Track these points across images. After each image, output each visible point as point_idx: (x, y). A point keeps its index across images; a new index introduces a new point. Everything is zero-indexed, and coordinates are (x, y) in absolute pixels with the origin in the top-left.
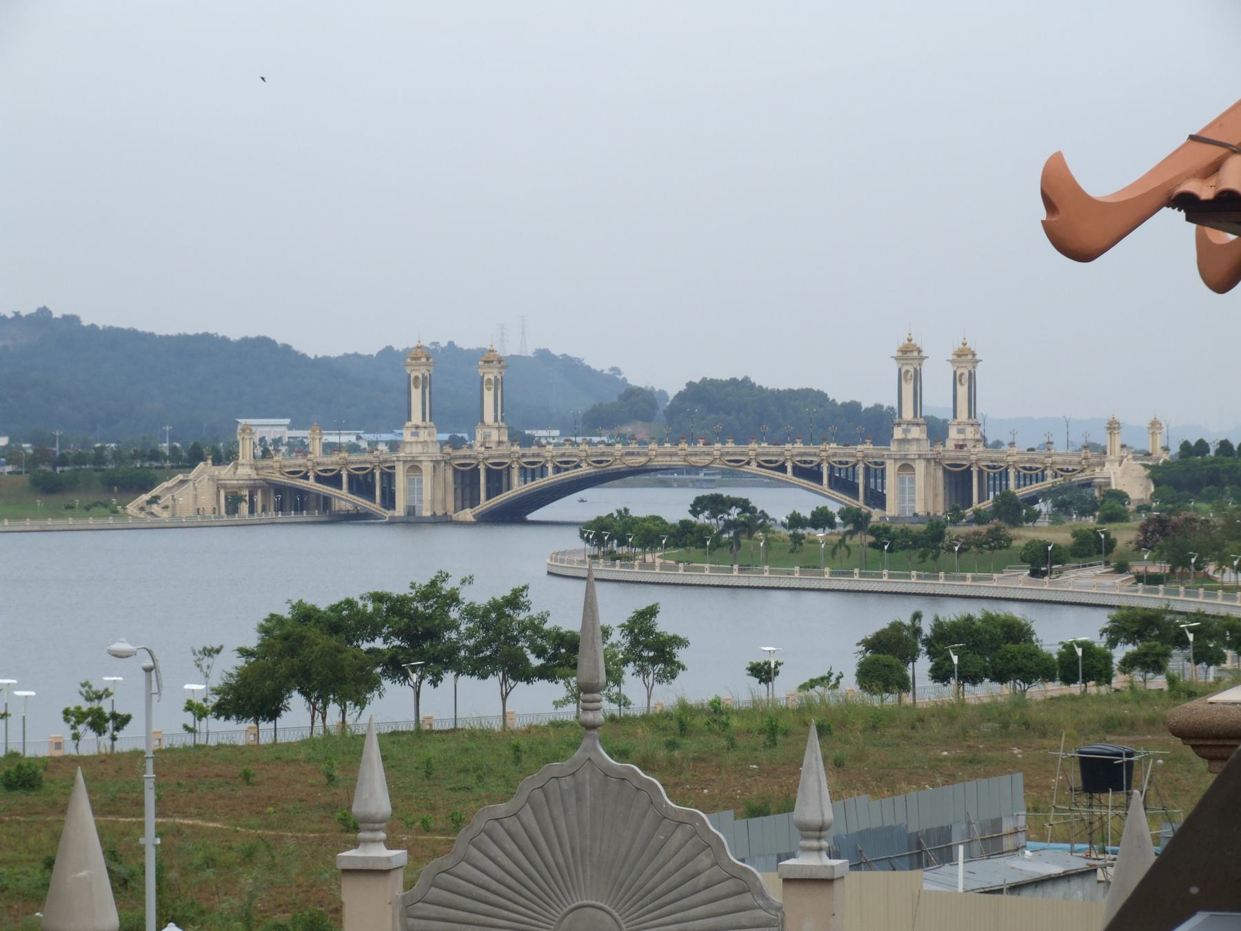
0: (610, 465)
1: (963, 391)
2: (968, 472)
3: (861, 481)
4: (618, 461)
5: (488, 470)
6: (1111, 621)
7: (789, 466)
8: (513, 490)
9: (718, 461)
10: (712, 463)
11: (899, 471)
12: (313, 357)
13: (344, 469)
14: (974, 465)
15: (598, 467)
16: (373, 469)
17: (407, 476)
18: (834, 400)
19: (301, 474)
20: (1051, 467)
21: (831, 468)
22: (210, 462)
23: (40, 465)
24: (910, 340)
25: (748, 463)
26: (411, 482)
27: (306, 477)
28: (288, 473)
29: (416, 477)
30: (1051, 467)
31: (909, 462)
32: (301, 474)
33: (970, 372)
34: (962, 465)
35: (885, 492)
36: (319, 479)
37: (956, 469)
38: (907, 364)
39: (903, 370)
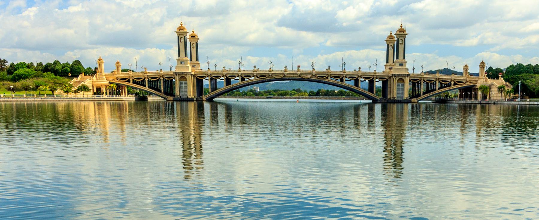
0: (267, 78)
2: (479, 76)
4: (270, 76)
5: (164, 81)
7: (131, 80)
8: (231, 85)
9: (314, 77)
10: (311, 77)
11: (397, 81)
13: (146, 78)
14: (146, 78)
15: (261, 79)
17: (180, 81)
19: (127, 80)
20: (241, 75)
22: (83, 74)
24: (181, 25)
25: (327, 78)
26: (181, 83)
27: (129, 81)
29: (183, 82)
30: (241, 75)
31: (184, 75)
32: (127, 80)
33: (196, 43)
34: (156, 78)
36: (134, 82)
37: (155, 79)
38: (401, 37)
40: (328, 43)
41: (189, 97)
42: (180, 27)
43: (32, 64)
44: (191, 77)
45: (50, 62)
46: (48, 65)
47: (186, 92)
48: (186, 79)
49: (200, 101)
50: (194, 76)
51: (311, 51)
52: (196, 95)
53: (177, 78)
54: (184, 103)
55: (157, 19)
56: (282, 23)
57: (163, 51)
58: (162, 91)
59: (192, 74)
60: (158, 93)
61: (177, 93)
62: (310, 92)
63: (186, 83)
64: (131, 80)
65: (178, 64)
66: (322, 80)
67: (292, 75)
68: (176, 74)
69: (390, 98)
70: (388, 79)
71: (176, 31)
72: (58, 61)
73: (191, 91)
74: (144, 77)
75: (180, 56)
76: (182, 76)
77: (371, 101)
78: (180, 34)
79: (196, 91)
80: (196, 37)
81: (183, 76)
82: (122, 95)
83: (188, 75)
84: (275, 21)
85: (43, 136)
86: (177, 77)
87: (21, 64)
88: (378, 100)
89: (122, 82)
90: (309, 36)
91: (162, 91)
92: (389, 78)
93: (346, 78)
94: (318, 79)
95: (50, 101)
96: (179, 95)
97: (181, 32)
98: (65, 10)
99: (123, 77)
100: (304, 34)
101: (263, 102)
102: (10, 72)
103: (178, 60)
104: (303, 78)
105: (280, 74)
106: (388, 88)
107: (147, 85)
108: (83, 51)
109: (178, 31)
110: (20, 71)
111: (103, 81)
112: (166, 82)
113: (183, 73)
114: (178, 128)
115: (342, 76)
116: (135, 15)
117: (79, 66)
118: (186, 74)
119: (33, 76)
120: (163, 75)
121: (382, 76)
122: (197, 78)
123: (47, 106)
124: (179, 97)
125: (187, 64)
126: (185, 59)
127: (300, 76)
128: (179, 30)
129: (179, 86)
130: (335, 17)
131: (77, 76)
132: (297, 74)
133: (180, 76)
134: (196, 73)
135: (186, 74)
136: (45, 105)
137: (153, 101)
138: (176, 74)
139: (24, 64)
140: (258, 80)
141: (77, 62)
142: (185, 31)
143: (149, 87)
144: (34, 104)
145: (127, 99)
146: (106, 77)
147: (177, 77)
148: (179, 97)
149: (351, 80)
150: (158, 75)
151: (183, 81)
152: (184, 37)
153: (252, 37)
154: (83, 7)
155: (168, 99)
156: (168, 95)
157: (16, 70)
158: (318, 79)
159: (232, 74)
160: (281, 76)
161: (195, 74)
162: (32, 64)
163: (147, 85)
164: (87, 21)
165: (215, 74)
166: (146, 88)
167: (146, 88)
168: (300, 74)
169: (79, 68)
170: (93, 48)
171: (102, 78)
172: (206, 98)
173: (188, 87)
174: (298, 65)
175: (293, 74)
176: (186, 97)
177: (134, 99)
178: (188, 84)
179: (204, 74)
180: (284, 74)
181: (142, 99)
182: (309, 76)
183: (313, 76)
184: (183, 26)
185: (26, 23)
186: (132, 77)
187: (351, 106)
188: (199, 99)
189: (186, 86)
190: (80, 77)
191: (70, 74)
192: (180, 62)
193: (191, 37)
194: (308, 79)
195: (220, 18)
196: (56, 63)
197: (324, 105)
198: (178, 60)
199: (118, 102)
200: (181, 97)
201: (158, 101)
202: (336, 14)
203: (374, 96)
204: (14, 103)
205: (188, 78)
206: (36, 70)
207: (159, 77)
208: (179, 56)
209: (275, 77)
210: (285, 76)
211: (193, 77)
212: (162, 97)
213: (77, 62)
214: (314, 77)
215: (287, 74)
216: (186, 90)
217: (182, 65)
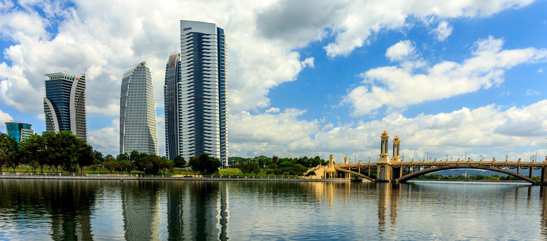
0: (444, 166)
1: (396, 149)
3: (369, 173)
6: (217, 200)
7: (350, 168)
9: (481, 166)
12: (463, 108)
15: (439, 167)
16: (368, 167)
18: (109, 156)
21: (361, 169)
22: (321, 165)
23: (525, 153)
24: (385, 132)
26: (381, 170)
27: (348, 169)
28: (536, 166)
33: (398, 144)
35: (376, 176)
36: (351, 170)
39: (383, 140)
40: (533, 144)
41: (386, 179)
42: (384, 134)
43: (291, 159)
44: (388, 166)
45: (301, 158)
46: (300, 159)
47: (385, 176)
48: (385, 167)
49: (394, 182)
50: (391, 165)
51: (521, 149)
52: (392, 179)
53: (379, 167)
54: (382, 184)
55: (410, 132)
56: (498, 131)
57: (413, 151)
58: (369, 175)
59: (389, 165)
60: (366, 177)
61: (378, 177)
62: (502, 177)
63: (385, 170)
64: (350, 168)
65: (380, 158)
66: (487, 168)
67: (463, 165)
68: (378, 164)
69: (545, 182)
70: (544, 167)
71: (381, 136)
72: (306, 157)
73: (388, 176)
74: (358, 167)
75: (382, 152)
76: (382, 165)
77: (531, 184)
78: (383, 138)
79: (392, 175)
80: (398, 140)
81: (383, 166)
82: (346, 178)
83: (386, 165)
84: (492, 130)
85: (293, 204)
86: (379, 166)
87: (285, 159)
88: (535, 183)
89: (344, 170)
90: (518, 139)
91: (369, 175)
92: (545, 166)
93: (534, 167)
94: (484, 167)
95: (216, 180)
96: (379, 178)
97: (384, 137)
98: (355, 129)
99: (345, 166)
100: (514, 137)
101: (442, 183)
102: (278, 164)
103: (380, 155)
104: (472, 167)
105: (454, 164)
106: (545, 174)
107: (359, 172)
108: (363, 152)
109: (382, 136)
110: (283, 163)
111: (332, 169)
112: (366, 170)
113: (383, 164)
114: (378, 199)
115: (530, 166)
116: (397, 130)
117: (318, 160)
118: (385, 164)
119: (289, 166)
120: (370, 165)
121: (539, 165)
122: (393, 167)
123: (99, 185)
124: (379, 179)
125: (386, 158)
126: (385, 154)
127: (469, 165)
128: (383, 136)
129: (380, 173)
130: (541, 125)
131: (316, 166)
132: (467, 164)
133: (381, 166)
134: (393, 164)
135: (385, 164)
136: (211, 184)
137: (279, 183)
138: (378, 164)
139: (287, 159)
140: (437, 168)
141: (317, 158)
142: (387, 136)
143: (361, 173)
144: (294, 183)
145: (348, 180)
146: (334, 167)
147: (379, 166)
148: (379, 179)
149: (539, 169)
150: (367, 165)
151: (383, 169)
152: (385, 140)
153: (474, 141)
154: (365, 126)
155: (372, 181)
156: (372, 178)
157: (281, 162)
158: (484, 167)
159: (442, 164)
160: (455, 165)
161: (392, 164)
162: (291, 159)
163: (359, 172)
164: (367, 134)
165: (406, 164)
166: (359, 174)
167: (359, 174)
168: (470, 164)
169: (318, 161)
170: (368, 151)
171: (331, 167)
172: (398, 181)
173: (386, 173)
174: (469, 157)
175: (465, 164)
176: (384, 179)
177: (350, 181)
178: (386, 171)
179: (398, 164)
180: (457, 164)
181: (356, 181)
182: (477, 165)
183: (480, 165)
184: (386, 133)
185: (331, 137)
186: (351, 166)
187: (512, 188)
188: (394, 181)
189: (385, 172)
190: (318, 166)
191: (54, 160)
192: (382, 157)
193: (395, 140)
194: (476, 167)
195: (454, 129)
196: (305, 158)
197: (485, 186)
198: (380, 155)
199: (295, 182)
200: (380, 179)
201: (343, 182)
202: (542, 123)
203: (531, 180)
204: (152, 181)
205: (386, 167)
206: (293, 163)
207: (368, 166)
208: (381, 153)
209: (450, 166)
210: (458, 165)
211: (390, 166)
212: (369, 179)
213: (317, 158)
214: (481, 166)
215: (460, 164)
216: (384, 175)
217: (383, 158)
